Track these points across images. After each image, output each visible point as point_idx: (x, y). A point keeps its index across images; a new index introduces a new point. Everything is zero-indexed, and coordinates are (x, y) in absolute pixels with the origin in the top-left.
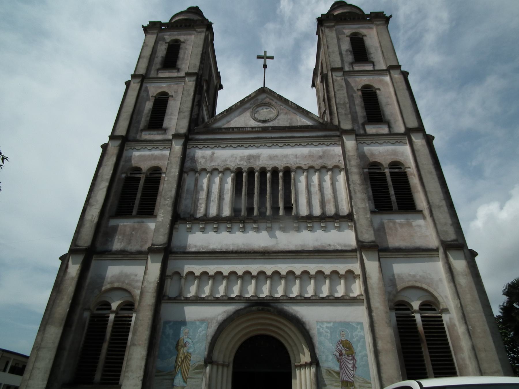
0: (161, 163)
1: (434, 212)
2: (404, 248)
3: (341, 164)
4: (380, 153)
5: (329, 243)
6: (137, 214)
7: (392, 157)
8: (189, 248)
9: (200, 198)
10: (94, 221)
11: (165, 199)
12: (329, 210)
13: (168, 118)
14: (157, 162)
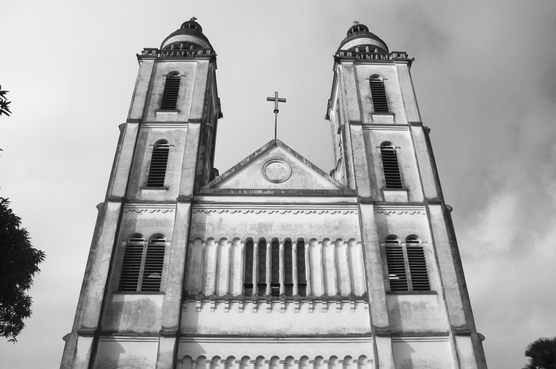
0: (165, 230)
1: (446, 295)
2: (417, 331)
3: (358, 236)
4: (398, 225)
5: (343, 326)
6: (142, 290)
7: (410, 230)
8: (199, 331)
9: (208, 272)
10: (98, 299)
11: (173, 276)
12: (344, 289)
13: (170, 174)
14: (160, 228)
